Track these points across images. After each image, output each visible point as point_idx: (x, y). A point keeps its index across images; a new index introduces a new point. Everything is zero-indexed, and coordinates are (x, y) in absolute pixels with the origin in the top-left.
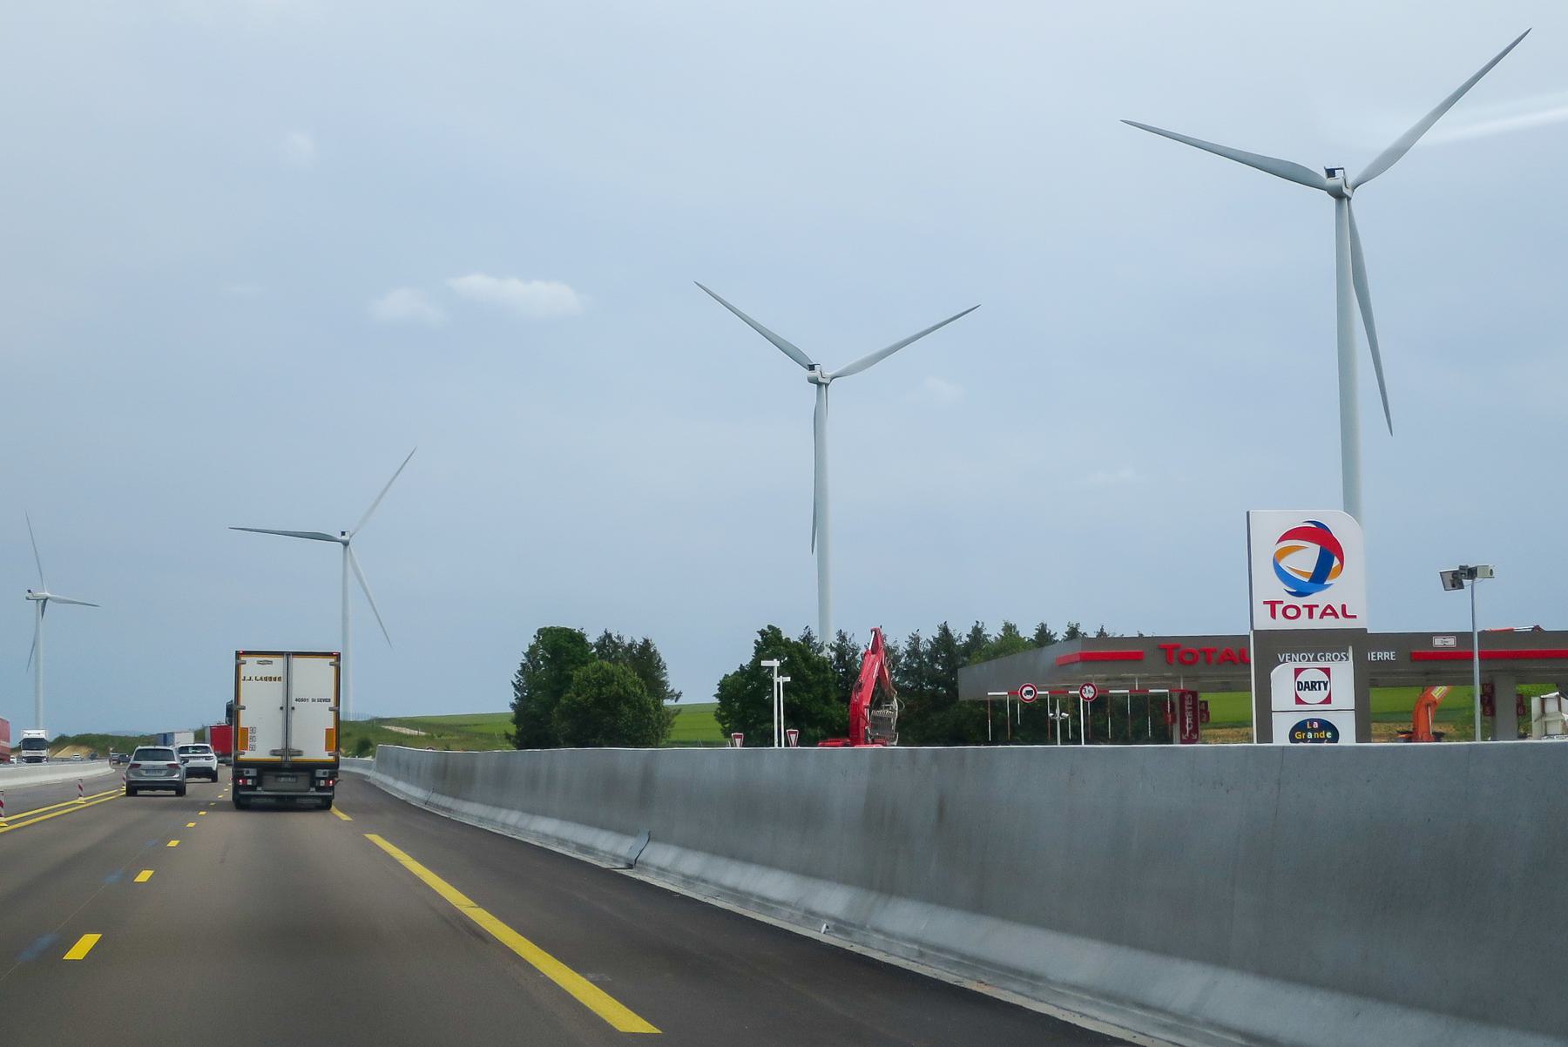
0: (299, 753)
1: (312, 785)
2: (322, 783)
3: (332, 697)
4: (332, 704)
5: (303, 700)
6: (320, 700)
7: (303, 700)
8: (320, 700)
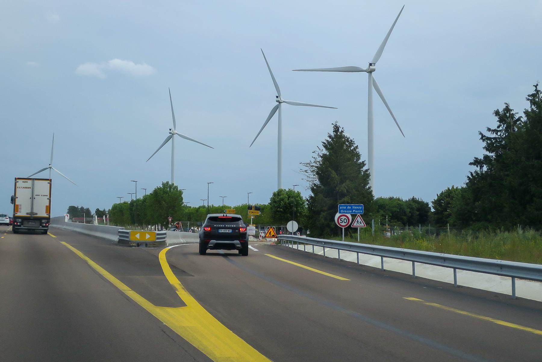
0: (36, 214)
1: (41, 225)
2: (44, 225)
3: (48, 195)
4: (48, 197)
5: (38, 195)
6: (44, 196)
7: (38, 195)
8: (44, 196)
